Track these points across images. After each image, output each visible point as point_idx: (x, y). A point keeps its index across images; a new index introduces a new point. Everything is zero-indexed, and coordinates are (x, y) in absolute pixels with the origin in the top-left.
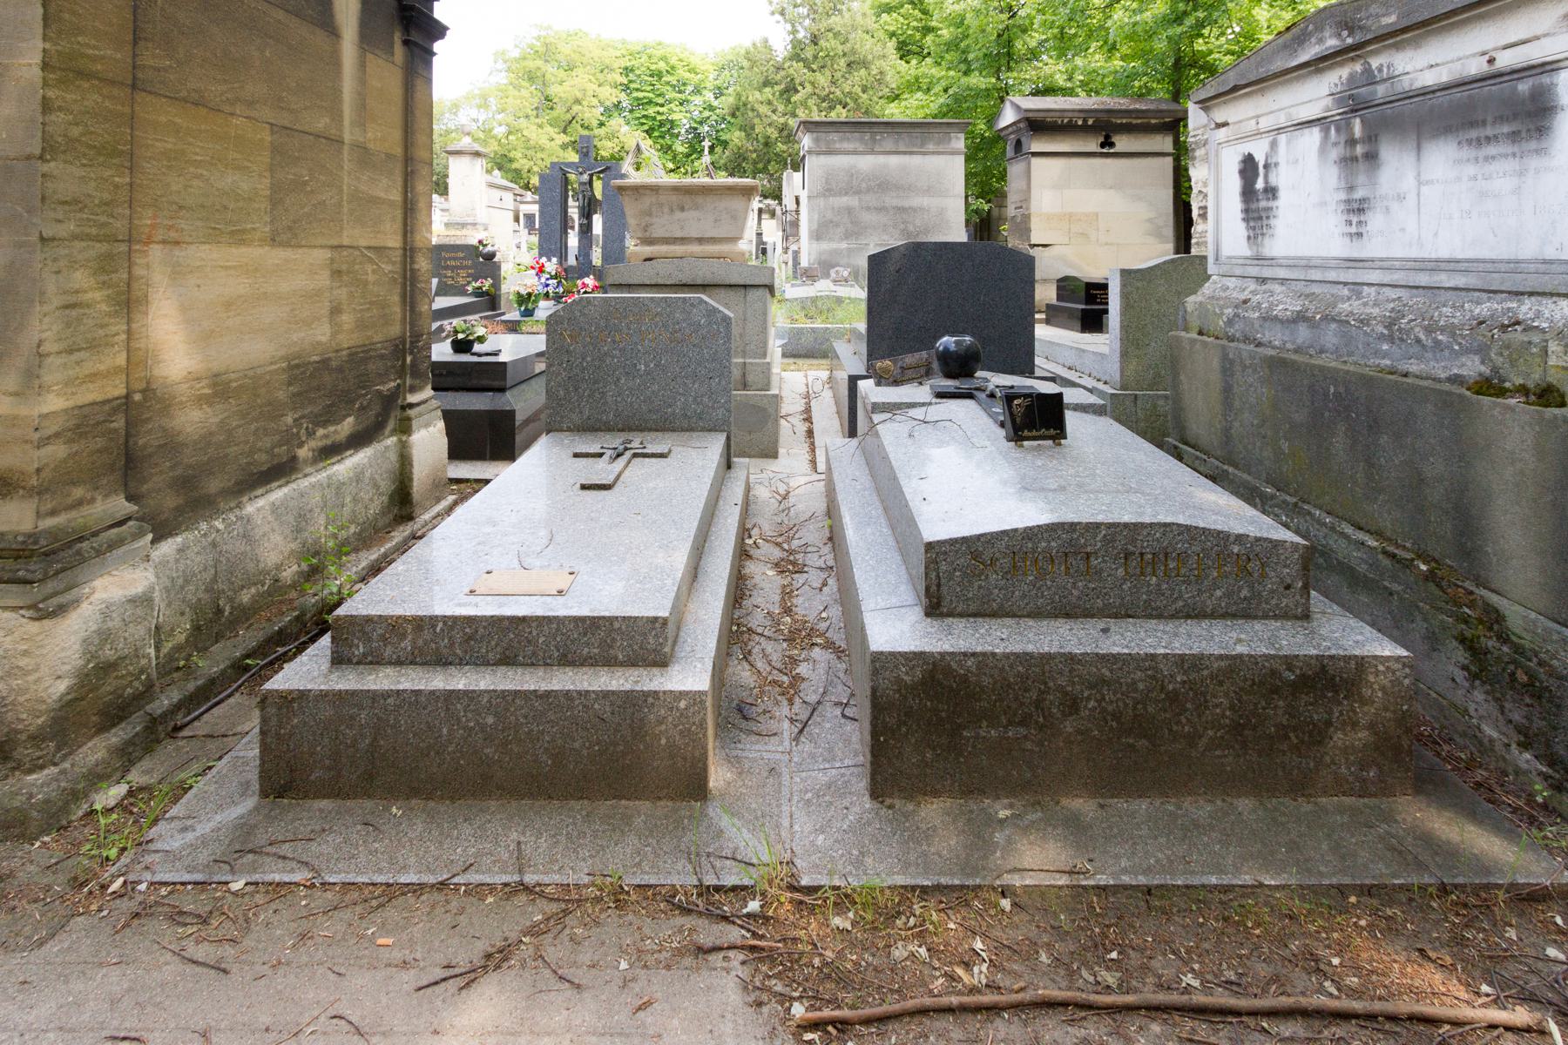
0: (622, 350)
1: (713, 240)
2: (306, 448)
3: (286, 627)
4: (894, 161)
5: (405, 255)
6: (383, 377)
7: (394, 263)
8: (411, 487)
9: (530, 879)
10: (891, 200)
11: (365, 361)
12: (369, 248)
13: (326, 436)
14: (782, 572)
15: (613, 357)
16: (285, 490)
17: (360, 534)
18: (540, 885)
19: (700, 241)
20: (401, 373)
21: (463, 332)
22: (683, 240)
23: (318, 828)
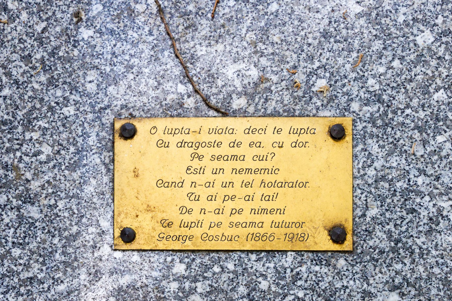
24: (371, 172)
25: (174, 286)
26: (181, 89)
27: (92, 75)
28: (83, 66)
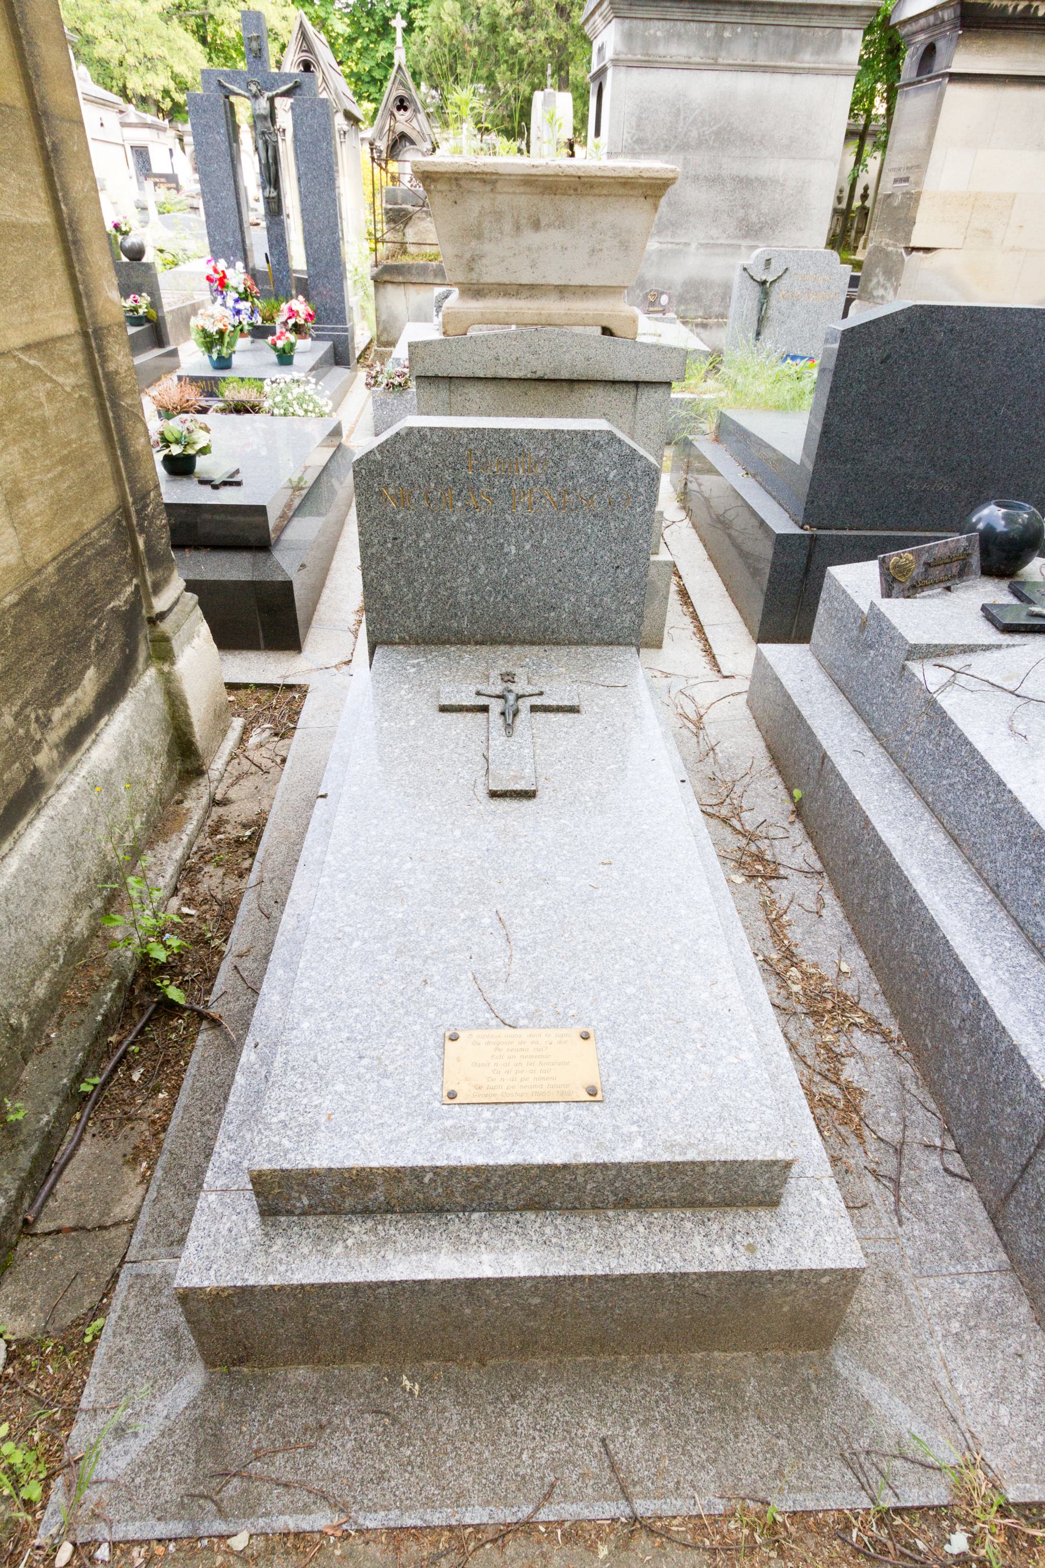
0: (481, 522)
1: (585, 291)
2: (45, 748)
3: (110, 1009)
4: (747, 83)
5: (88, 347)
6: (112, 586)
7: (75, 368)
8: (192, 734)
9: (644, 1507)
10: (732, 165)
11: (81, 571)
12: (27, 348)
13: (67, 715)
14: (753, 877)
15: (466, 533)
16: (40, 824)
17: (148, 821)
18: (660, 1518)
19: (562, 291)
20: (136, 567)
21: (177, 442)
22: (532, 290)
23: (311, 1421)
24: (609, 1057)
25: (483, 1125)
26: (487, 1015)
27: (432, 1009)
28: (427, 1005)
